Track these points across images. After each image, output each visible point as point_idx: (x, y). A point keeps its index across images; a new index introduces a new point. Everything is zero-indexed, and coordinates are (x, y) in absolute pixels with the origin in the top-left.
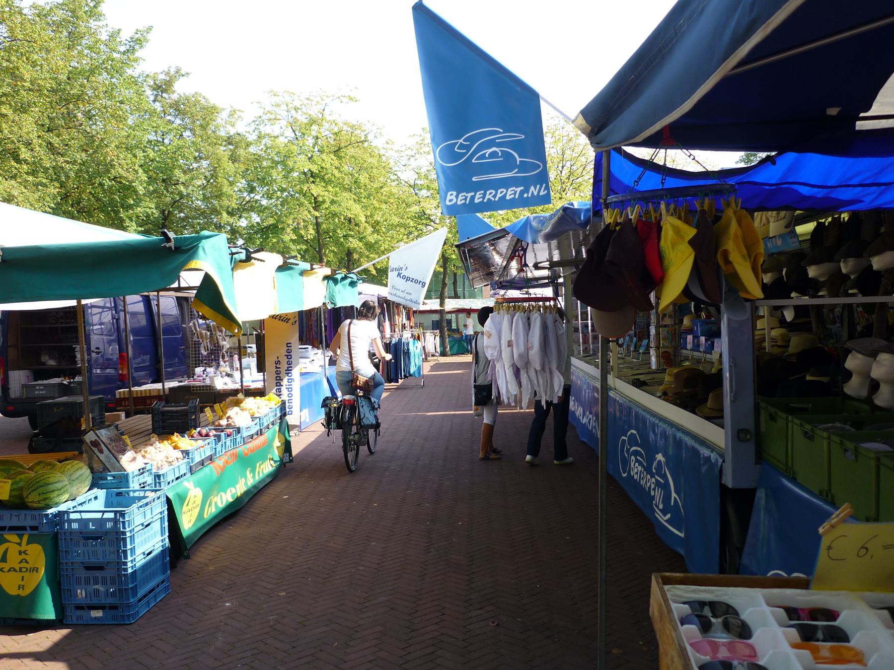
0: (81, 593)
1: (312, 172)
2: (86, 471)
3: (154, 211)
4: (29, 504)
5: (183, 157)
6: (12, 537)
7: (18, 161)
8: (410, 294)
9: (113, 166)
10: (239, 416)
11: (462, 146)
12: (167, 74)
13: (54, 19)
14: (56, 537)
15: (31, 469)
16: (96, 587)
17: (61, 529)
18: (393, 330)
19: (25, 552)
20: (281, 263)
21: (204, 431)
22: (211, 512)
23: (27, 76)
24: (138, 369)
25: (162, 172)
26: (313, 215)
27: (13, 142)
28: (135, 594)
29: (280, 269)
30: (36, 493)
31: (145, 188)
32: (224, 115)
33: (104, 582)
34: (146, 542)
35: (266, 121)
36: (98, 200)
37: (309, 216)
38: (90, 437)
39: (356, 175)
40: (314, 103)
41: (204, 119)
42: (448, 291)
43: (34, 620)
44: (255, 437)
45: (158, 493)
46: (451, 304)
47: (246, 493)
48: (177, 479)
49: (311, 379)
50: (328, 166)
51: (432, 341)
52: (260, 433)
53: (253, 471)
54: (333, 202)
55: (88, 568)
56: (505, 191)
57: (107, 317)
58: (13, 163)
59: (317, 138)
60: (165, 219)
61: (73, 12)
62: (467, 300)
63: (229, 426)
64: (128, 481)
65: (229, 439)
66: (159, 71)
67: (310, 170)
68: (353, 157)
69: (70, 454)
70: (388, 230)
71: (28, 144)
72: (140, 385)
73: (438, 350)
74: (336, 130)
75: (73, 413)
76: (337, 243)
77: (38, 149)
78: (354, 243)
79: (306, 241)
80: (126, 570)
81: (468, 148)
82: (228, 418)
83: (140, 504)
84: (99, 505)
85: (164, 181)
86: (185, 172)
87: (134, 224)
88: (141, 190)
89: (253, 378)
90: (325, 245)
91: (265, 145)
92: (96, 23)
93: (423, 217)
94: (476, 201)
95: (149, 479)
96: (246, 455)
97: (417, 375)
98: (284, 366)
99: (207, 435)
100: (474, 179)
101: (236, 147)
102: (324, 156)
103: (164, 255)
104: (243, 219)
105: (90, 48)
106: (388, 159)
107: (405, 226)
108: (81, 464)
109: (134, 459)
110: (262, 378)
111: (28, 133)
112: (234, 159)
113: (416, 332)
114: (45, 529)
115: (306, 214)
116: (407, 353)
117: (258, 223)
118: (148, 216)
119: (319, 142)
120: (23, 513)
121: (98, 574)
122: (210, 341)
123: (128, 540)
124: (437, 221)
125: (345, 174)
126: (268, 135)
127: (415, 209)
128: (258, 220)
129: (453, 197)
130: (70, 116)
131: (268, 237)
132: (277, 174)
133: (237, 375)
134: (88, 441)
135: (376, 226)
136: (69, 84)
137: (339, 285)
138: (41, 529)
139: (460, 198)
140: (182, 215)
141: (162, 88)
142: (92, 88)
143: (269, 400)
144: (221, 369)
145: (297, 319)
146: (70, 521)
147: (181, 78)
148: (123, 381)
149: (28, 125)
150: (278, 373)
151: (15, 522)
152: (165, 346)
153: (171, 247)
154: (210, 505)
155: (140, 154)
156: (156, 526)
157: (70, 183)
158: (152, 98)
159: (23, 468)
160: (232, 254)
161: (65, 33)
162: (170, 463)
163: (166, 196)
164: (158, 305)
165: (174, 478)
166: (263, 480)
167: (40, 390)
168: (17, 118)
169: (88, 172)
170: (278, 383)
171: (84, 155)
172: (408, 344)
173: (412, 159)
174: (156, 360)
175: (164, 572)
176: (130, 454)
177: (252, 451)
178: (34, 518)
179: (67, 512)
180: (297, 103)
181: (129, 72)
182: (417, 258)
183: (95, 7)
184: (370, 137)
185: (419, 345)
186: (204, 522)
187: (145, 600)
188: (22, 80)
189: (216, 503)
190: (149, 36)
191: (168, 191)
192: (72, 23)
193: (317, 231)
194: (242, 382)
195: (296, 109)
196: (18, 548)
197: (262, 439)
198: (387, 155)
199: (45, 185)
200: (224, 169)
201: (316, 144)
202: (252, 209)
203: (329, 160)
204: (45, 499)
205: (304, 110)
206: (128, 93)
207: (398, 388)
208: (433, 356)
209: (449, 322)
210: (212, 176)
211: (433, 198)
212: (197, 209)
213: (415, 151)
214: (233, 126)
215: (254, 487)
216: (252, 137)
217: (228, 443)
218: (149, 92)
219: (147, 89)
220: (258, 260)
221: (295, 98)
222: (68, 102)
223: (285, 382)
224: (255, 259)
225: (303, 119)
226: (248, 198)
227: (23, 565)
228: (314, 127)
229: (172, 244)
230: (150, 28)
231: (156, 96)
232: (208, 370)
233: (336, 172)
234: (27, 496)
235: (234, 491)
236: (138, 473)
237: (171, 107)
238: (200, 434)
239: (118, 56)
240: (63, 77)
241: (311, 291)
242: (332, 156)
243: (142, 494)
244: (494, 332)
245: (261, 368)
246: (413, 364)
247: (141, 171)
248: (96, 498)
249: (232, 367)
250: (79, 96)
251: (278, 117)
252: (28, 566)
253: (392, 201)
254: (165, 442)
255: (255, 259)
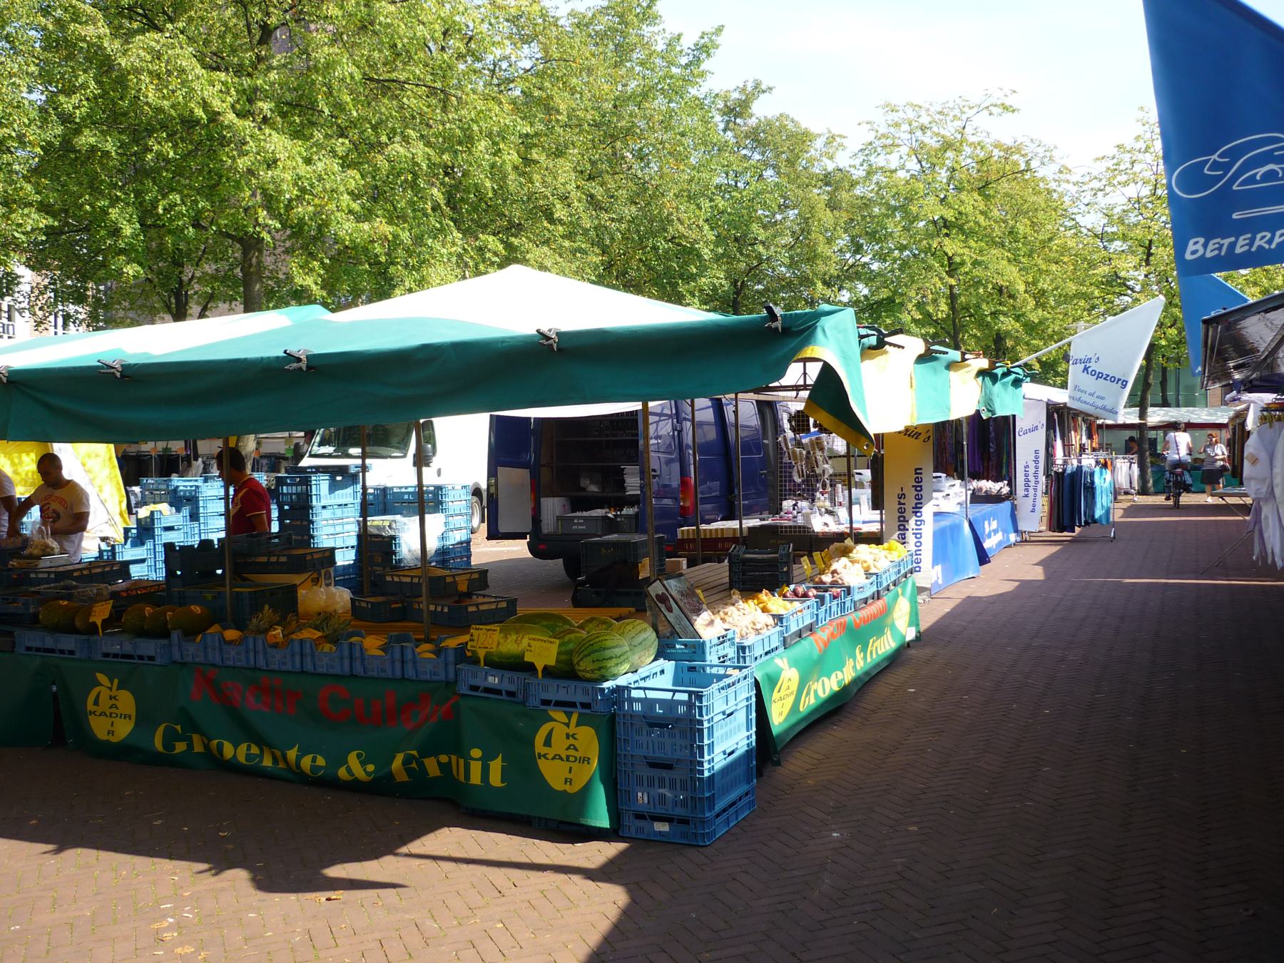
0: (642, 797)
1: (945, 220)
2: (650, 635)
3: (724, 282)
4: (581, 674)
5: (765, 205)
6: (559, 715)
7: (551, 220)
8: (1103, 398)
9: (670, 222)
10: (850, 570)
11: (1216, 165)
12: (743, 90)
13: (597, 28)
14: (613, 718)
15: (581, 627)
16: (661, 791)
17: (620, 709)
18: (1067, 453)
19: (573, 736)
20: (922, 351)
21: (801, 590)
22: (809, 703)
23: (562, 107)
24: (704, 501)
25: (735, 228)
26: (945, 284)
27: (546, 197)
28: (712, 808)
29: (921, 359)
30: (589, 659)
31: (712, 251)
32: (819, 143)
33: (672, 786)
34: (728, 739)
35: (879, 149)
36: (650, 269)
37: (939, 285)
38: (656, 589)
39: (1011, 223)
40: (950, 118)
41: (792, 151)
42: (1154, 394)
43: (582, 825)
44: (870, 601)
45: (745, 672)
46: (1156, 416)
47: (855, 682)
48: (766, 654)
49: (945, 523)
50: (969, 209)
51: (1126, 470)
52: (877, 596)
53: (864, 650)
54: (976, 263)
55: (653, 765)
56: (1269, 235)
57: (666, 428)
58: (546, 224)
59: (954, 170)
60: (738, 293)
61: (621, 16)
62: (1184, 409)
63: (834, 584)
64: (704, 653)
65: (835, 602)
66: (731, 89)
67: (942, 217)
68: (1006, 195)
69: (625, 611)
70: (1058, 303)
71: (564, 198)
72: (709, 522)
73: (1136, 485)
74: (982, 155)
75: (627, 558)
76: (982, 324)
77: (576, 204)
78: (1007, 324)
79: (936, 321)
80: (702, 772)
81: (1226, 167)
82: (834, 572)
83: (722, 684)
84: (666, 681)
85: (736, 240)
86: (765, 227)
87: (696, 300)
88: (706, 253)
89: (866, 517)
90: (963, 327)
91: (877, 183)
92: (650, 29)
93: (1115, 282)
94: (1238, 250)
95: (731, 652)
96: (858, 626)
97: (1104, 522)
98: (910, 502)
99: (805, 595)
100: (1235, 216)
101: (836, 189)
102: (963, 196)
103: (765, 340)
104: (844, 292)
105: (642, 64)
106: (1061, 196)
107: (1087, 297)
108: (646, 625)
109: (711, 623)
110: (878, 518)
111: (563, 184)
112: (833, 205)
113: (1102, 456)
114: (599, 708)
115: (937, 282)
116: (1091, 489)
117: (865, 296)
118: (715, 289)
119: (957, 175)
120: (573, 684)
121: (665, 774)
122: (807, 464)
123: (706, 732)
124: (1138, 288)
125: (996, 221)
126: (882, 168)
127: (1103, 270)
128: (866, 291)
129: (1199, 247)
130: (616, 158)
131: (880, 317)
132: (894, 225)
133: (842, 513)
134: (653, 595)
135: (1040, 298)
136: (615, 114)
137: (998, 384)
138: (595, 708)
139: (1210, 247)
140: (760, 287)
141: (736, 110)
142: (645, 117)
143: (889, 549)
144: (818, 504)
145: (930, 434)
146: (631, 700)
147: (762, 96)
148: (686, 516)
149: (565, 174)
150: (902, 511)
151: (562, 696)
152: (747, 470)
153: (300, 369)
154: (808, 693)
155: (706, 204)
156: (741, 716)
157: (615, 249)
158: (722, 126)
159: (571, 625)
160: (861, 337)
161: (611, 47)
162: (758, 631)
163: (739, 261)
164: (736, 412)
165: (762, 652)
166: (878, 664)
167: (579, 524)
168: (551, 165)
169: (638, 231)
170: (902, 527)
171: (633, 209)
172: (1092, 474)
173: (1100, 194)
174: (729, 487)
175: (749, 781)
176: (706, 616)
177: (865, 622)
178: (586, 692)
179: (628, 688)
180: (925, 120)
181: (693, 91)
182: (1117, 342)
183: (649, 7)
184: (1034, 164)
185: (1108, 475)
186: (799, 717)
187: (725, 816)
188: (558, 112)
189: (816, 691)
190: (719, 40)
191: (742, 254)
192: (619, 31)
193: (952, 306)
194: (851, 522)
195: (923, 129)
196: (566, 730)
197: (880, 603)
198: (1059, 190)
199: (584, 252)
200: (820, 220)
201: (951, 178)
202: (858, 276)
203: (971, 202)
204: (600, 668)
205: (935, 129)
206: (690, 122)
207: (1074, 541)
208: (1126, 493)
209: (1153, 443)
210: (803, 230)
211: (1133, 253)
212: (781, 278)
213: (1104, 182)
214: (831, 158)
215: (866, 673)
216: (859, 173)
217: (834, 608)
218: (718, 118)
219: (714, 113)
220: (895, 345)
221: (923, 113)
222: (614, 138)
223: (912, 523)
224: (891, 344)
225: (931, 142)
226: (851, 262)
227: (571, 752)
228: (950, 154)
229: (778, 324)
230: (720, 30)
231: (728, 122)
232: (800, 504)
233: (981, 219)
234: (578, 663)
235: (840, 676)
236: (716, 641)
237: (746, 137)
238: (795, 593)
239: (679, 71)
240: (608, 106)
241: (961, 394)
242: (976, 195)
243: (722, 671)
244: (1263, 456)
245: (877, 503)
246: (1098, 505)
247: (706, 227)
248: (662, 672)
249: (833, 501)
250: (629, 129)
251: (897, 141)
252: (578, 755)
253: (1066, 259)
254: (750, 602)
255: (891, 344)
